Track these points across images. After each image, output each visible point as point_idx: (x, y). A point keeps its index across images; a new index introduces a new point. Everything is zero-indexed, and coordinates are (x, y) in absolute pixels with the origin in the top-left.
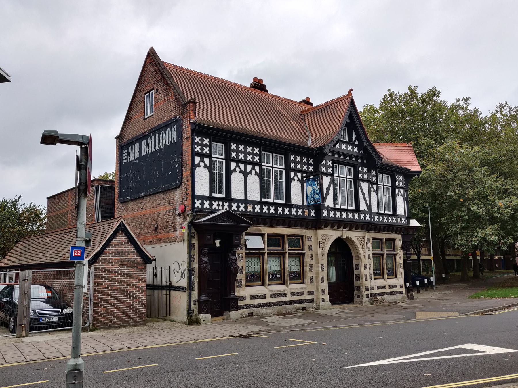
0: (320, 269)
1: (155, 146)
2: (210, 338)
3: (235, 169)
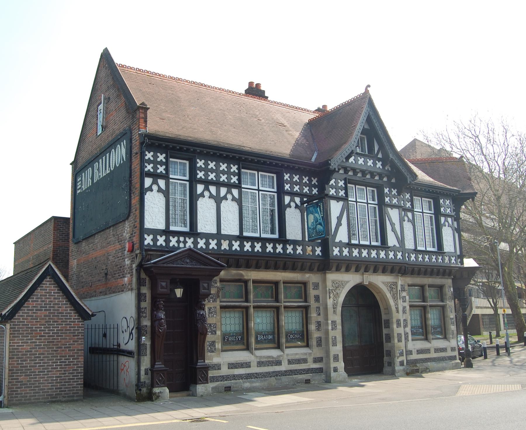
0: (330, 328)
1: (106, 169)
2: (164, 420)
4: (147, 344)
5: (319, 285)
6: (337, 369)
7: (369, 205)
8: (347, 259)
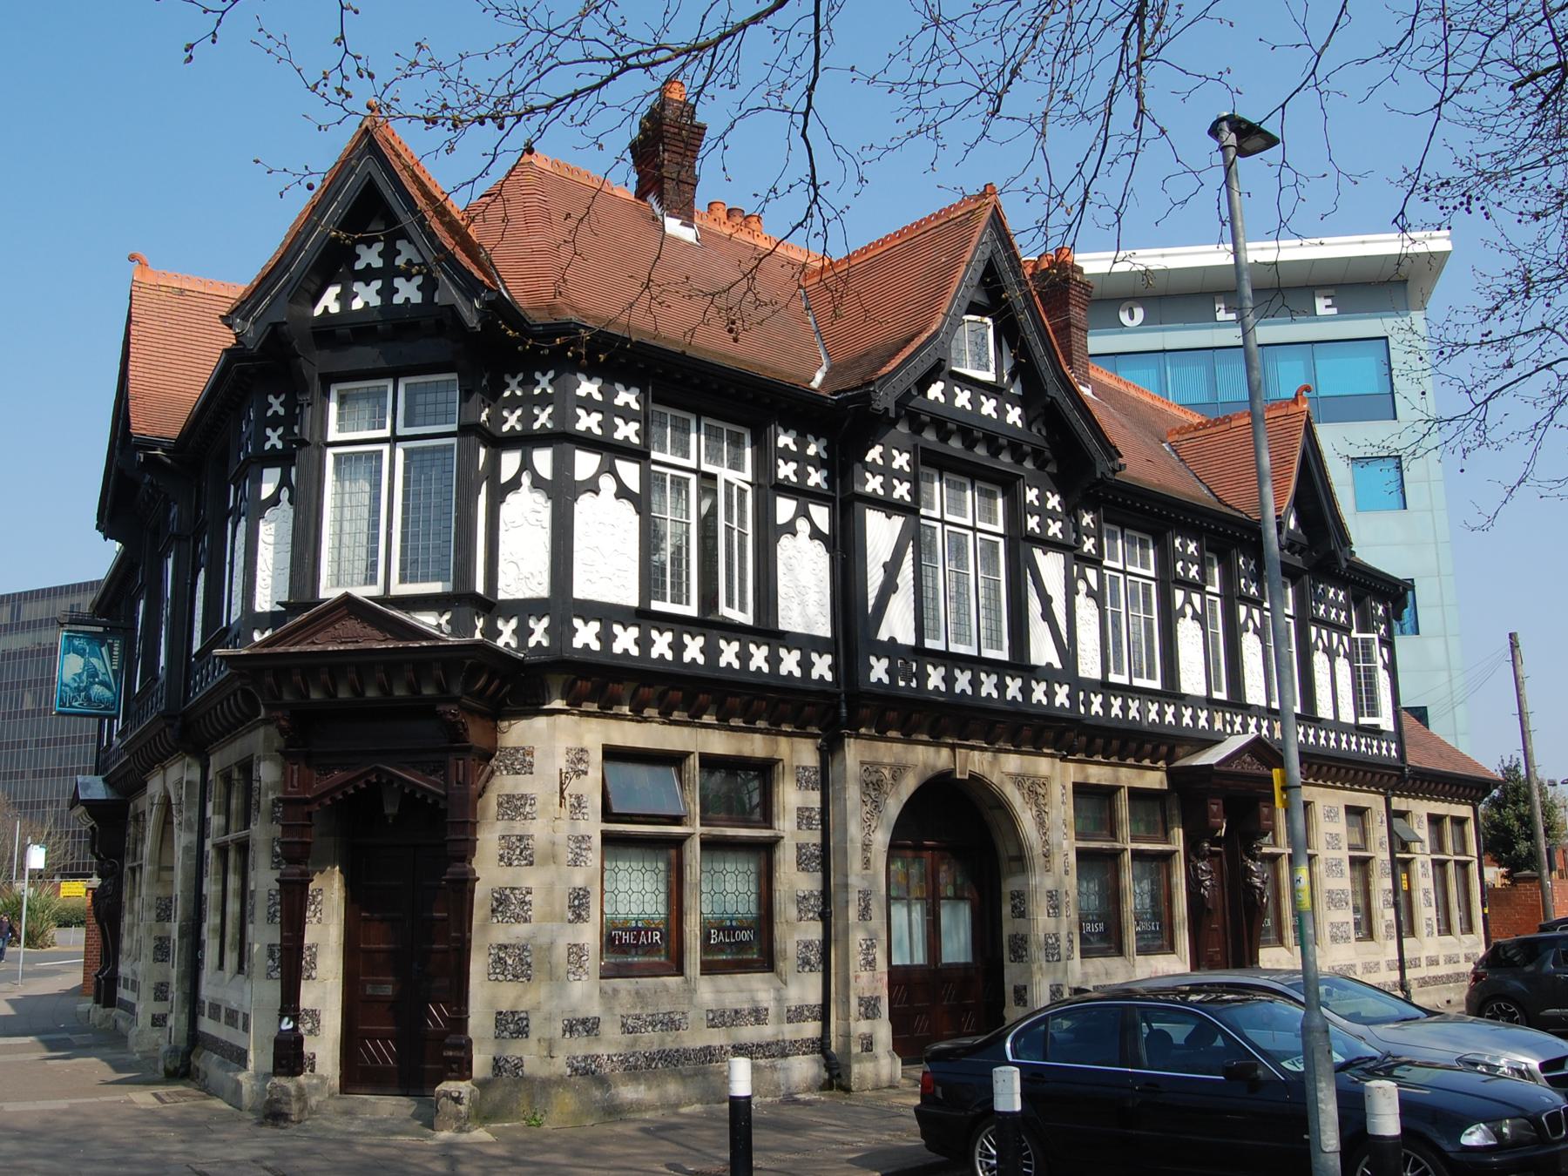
8: (1064, 714)
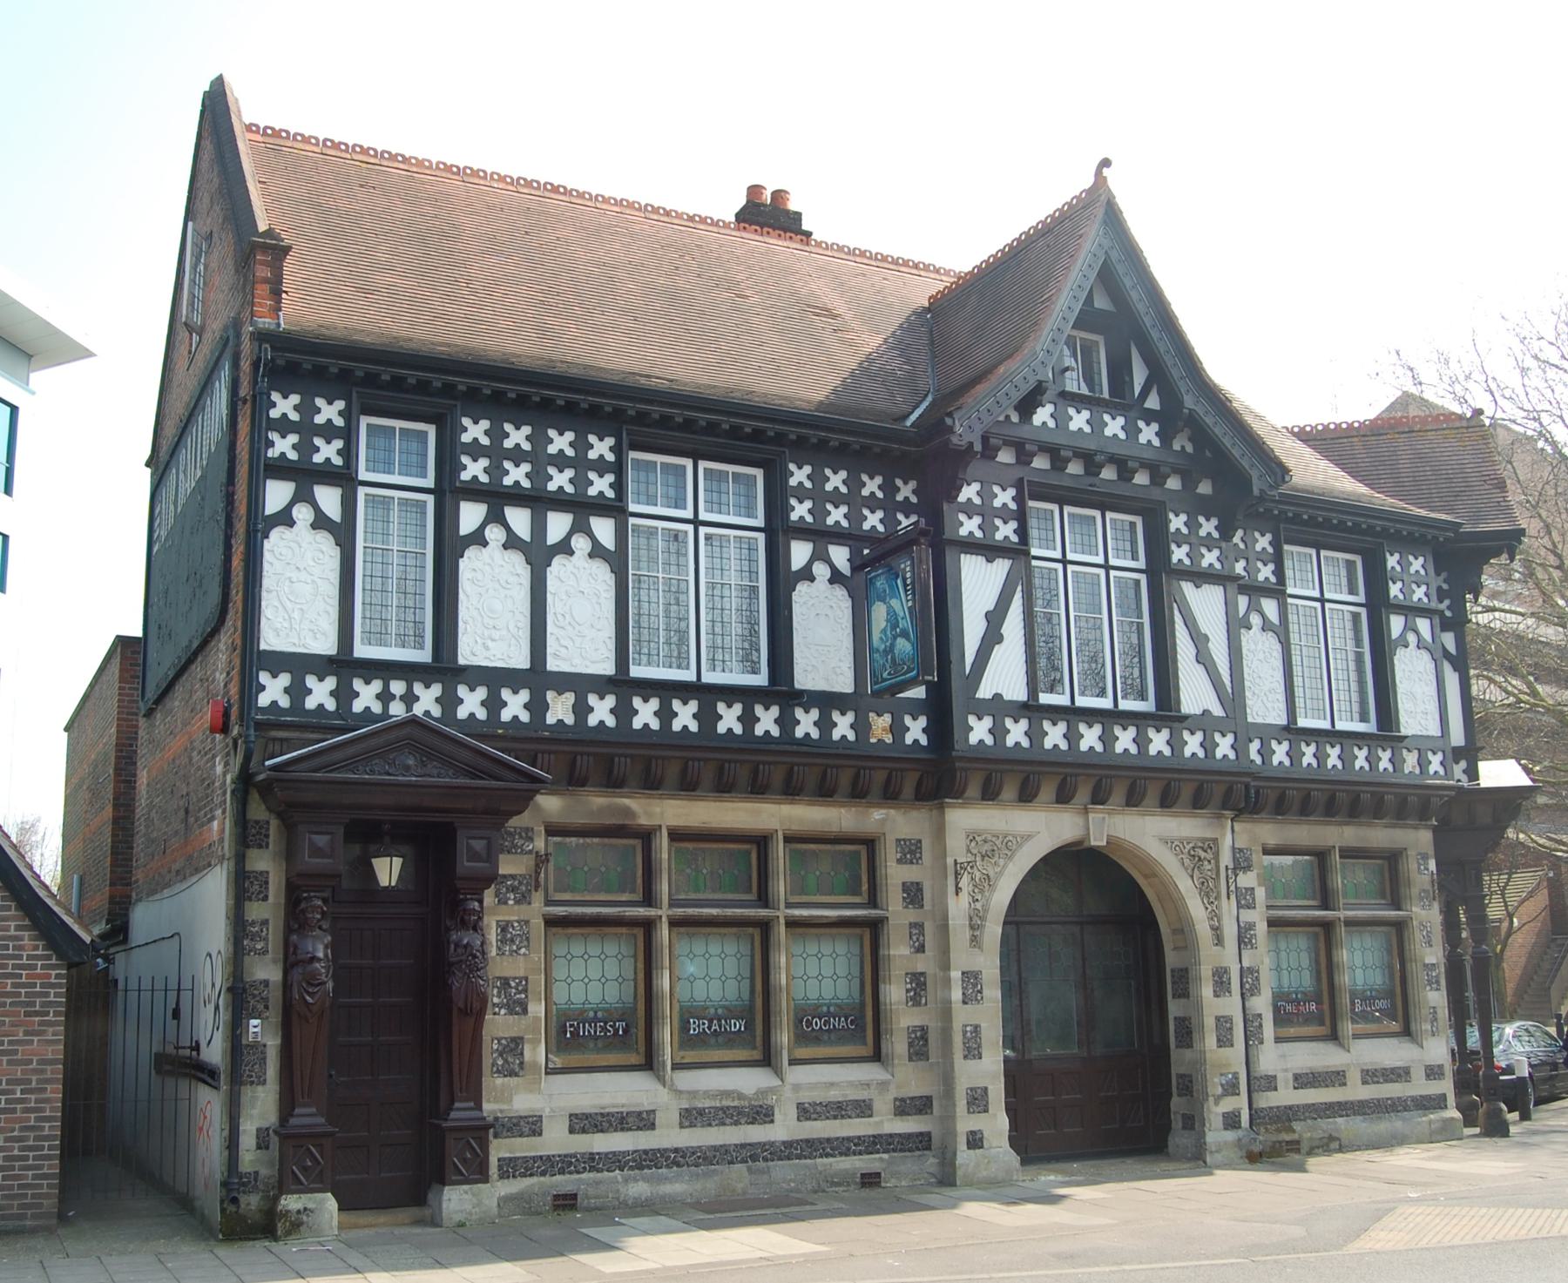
0: (956, 994)
3: (287, 510)
4: (269, 1043)
5: (921, 848)
6: (981, 1140)
7: (1113, 573)
8: (1095, 761)
